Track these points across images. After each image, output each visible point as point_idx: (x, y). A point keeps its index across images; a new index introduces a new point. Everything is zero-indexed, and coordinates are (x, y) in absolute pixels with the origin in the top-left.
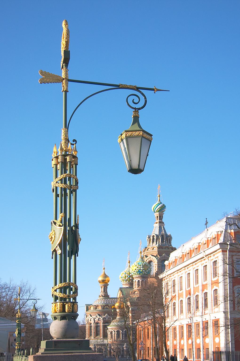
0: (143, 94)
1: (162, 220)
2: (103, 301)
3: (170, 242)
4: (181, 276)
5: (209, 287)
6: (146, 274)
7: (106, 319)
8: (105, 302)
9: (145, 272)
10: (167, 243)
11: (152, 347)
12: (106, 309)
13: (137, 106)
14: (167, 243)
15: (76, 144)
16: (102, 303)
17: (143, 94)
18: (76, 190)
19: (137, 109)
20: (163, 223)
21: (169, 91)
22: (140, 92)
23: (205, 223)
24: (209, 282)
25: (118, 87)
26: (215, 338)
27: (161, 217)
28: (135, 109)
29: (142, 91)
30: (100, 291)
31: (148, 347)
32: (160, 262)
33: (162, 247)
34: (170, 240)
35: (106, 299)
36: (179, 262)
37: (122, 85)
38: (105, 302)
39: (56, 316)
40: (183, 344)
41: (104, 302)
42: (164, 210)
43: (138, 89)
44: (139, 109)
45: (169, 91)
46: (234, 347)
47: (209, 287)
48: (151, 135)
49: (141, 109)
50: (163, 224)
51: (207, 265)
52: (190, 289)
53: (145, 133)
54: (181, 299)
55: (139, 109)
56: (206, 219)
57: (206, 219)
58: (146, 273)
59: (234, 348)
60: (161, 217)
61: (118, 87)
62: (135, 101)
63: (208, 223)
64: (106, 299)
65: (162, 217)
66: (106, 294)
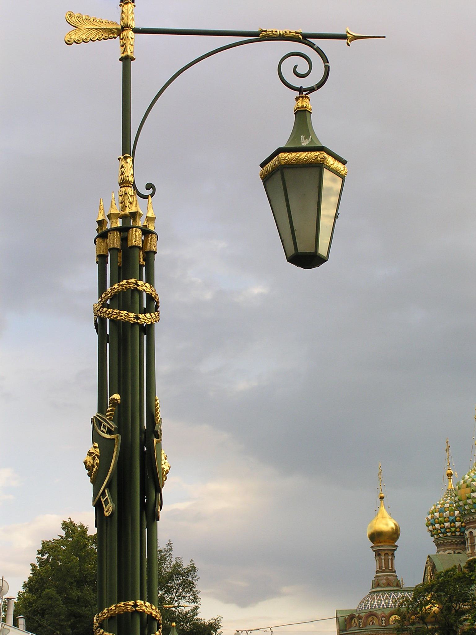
0: (319, 51)
2: (385, 600)
8: (391, 602)
13: (306, 83)
15: (152, 195)
16: (383, 605)
17: (319, 51)
19: (305, 90)
21: (385, 37)
22: (312, 45)
28: (300, 90)
29: (317, 42)
35: (393, 594)
37: (265, 31)
38: (391, 602)
39: (25, 631)
41: (387, 601)
43: (305, 39)
44: (311, 90)
45: (385, 37)
49: (316, 88)
51: (371, 547)
52: (196, 608)
53: (330, 157)
55: (311, 90)
62: (300, 71)
64: (393, 594)
66: (392, 577)
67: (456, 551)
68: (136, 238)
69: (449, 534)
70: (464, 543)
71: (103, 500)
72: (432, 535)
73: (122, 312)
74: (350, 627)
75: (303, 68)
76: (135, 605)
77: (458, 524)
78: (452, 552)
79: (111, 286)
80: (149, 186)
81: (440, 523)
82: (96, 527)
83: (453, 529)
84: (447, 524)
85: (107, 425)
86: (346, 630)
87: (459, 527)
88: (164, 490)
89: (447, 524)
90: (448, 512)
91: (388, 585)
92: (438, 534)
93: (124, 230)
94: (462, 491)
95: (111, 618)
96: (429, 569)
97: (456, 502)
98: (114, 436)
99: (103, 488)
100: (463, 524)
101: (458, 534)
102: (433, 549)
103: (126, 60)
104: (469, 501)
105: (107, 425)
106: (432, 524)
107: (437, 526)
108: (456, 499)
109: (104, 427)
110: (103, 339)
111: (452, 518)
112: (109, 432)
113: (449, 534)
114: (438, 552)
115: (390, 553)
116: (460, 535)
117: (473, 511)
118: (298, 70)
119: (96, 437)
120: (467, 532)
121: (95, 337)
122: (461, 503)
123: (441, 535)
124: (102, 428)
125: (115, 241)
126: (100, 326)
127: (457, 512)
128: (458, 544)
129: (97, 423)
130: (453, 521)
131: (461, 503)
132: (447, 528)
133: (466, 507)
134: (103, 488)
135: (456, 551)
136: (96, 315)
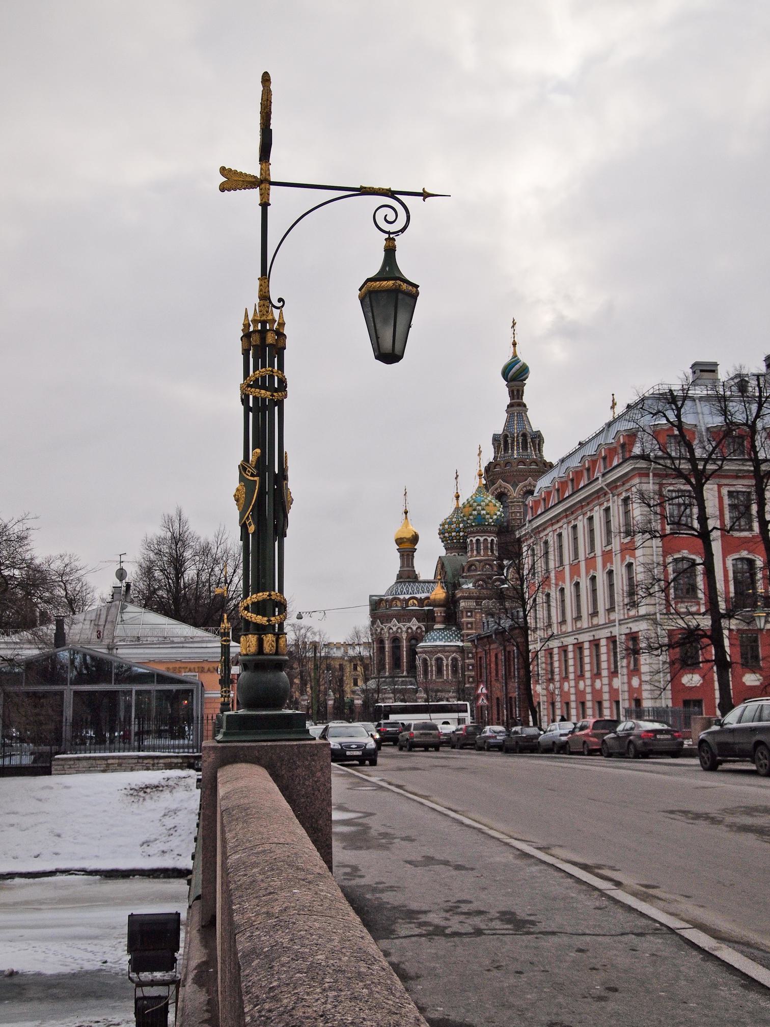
1: (522, 399)
3: (540, 450)
4: (558, 531)
5: (617, 559)
6: (493, 524)
7: (411, 628)
9: (491, 520)
10: (535, 451)
11: (200, 728)
12: (412, 606)
14: (533, 453)
15: (282, 306)
18: (282, 401)
20: (525, 406)
23: (611, 404)
24: (616, 545)
25: (364, 191)
26: (632, 679)
27: (521, 392)
28: (389, 233)
30: (395, 563)
31: (498, 699)
32: (520, 496)
33: (523, 462)
34: (539, 445)
36: (556, 498)
40: (637, 686)
42: (525, 376)
43: (391, 194)
46: (671, 697)
47: (617, 559)
48: (417, 286)
50: (524, 409)
54: (576, 579)
56: (613, 395)
57: (613, 395)
58: (493, 522)
59: (670, 701)
60: (521, 392)
61: (364, 191)
62: (390, 219)
63: (616, 404)
65: (523, 392)
67: (460, 554)
68: (271, 338)
69: (455, 541)
70: (466, 548)
71: (247, 523)
72: (442, 542)
73: (262, 391)
74: (380, 608)
75: (391, 217)
76: (270, 595)
77: (462, 534)
78: (457, 554)
79: (254, 372)
80: (280, 300)
81: (449, 533)
82: (241, 540)
83: (458, 538)
84: (454, 534)
85: (251, 470)
86: (376, 610)
87: (463, 536)
88: (289, 515)
89: (454, 534)
90: (455, 525)
91: (409, 577)
92: (447, 541)
93: (263, 333)
94: (466, 509)
95: (253, 603)
96: (439, 566)
97: (461, 517)
98: (256, 478)
99: (248, 512)
100: (466, 534)
101: (461, 541)
102: (443, 552)
103: (265, 205)
104: (471, 517)
105: (251, 470)
106: (443, 534)
107: (446, 535)
108: (462, 515)
109: (249, 471)
110: (247, 410)
111: (457, 529)
112: (252, 475)
113: (455, 541)
114: (447, 554)
115: (411, 554)
116: (457, 542)
117: (473, 524)
118: (387, 218)
119: (242, 478)
120: (468, 540)
121: (241, 408)
122: (465, 519)
123: (449, 542)
124: (247, 472)
125: (256, 339)
126: (245, 401)
127: (461, 525)
128: (461, 548)
129: (243, 468)
130: (459, 532)
131: (465, 519)
132: (454, 536)
133: (469, 521)
134: (248, 512)
135: (460, 554)
136: (242, 391)
